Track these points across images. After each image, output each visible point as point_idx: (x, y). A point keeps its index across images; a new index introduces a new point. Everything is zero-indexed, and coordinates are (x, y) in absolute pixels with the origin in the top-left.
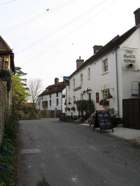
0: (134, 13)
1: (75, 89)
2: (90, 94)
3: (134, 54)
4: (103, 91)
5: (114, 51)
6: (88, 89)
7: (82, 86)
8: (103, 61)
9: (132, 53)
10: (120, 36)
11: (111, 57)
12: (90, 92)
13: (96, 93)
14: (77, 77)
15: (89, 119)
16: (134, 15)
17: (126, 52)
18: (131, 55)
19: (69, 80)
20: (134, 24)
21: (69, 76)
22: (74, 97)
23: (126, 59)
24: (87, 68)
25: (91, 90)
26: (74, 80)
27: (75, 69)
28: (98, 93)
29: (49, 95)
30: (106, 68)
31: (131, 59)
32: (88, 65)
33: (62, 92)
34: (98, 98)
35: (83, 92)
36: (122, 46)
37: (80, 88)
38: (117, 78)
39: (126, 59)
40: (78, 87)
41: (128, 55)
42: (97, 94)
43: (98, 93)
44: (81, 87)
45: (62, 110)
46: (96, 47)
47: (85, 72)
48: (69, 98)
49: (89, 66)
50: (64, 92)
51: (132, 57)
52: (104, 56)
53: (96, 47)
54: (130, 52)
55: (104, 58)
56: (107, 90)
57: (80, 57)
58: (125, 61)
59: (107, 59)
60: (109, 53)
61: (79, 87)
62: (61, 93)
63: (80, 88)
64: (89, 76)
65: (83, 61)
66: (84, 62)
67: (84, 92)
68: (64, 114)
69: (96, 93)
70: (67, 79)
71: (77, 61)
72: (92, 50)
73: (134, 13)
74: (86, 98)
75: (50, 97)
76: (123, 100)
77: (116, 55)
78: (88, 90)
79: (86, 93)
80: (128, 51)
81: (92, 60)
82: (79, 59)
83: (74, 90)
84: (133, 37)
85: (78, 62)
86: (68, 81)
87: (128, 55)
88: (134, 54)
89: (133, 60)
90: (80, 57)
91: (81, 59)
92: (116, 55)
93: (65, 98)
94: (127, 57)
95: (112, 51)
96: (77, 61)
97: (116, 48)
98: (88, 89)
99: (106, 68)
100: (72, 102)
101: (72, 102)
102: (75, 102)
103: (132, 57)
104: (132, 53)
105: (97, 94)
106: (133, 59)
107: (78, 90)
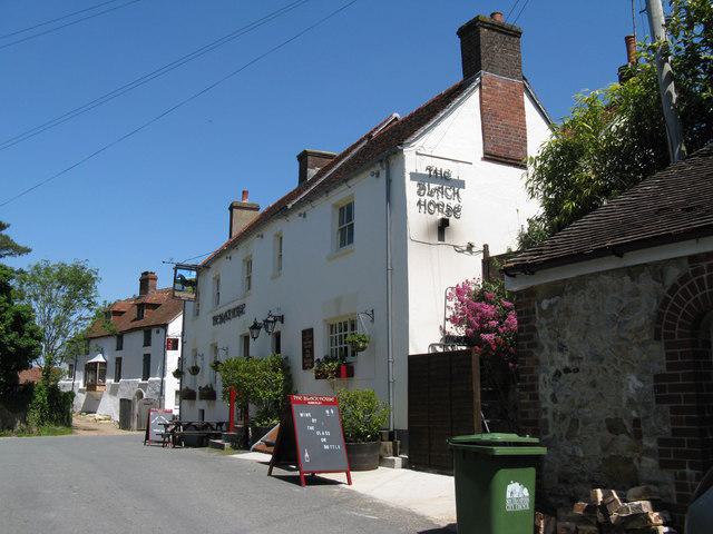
12: (278, 326)
13: (304, 332)
14: (231, 271)
21: (200, 262)
25: (282, 319)
30: (346, 235)
31: (446, 201)
37: (239, 311)
40: (231, 306)
42: (308, 335)
58: (423, 208)
63: (239, 311)
67: (256, 327)
69: (304, 332)
70: (191, 276)
81: (280, 210)
83: (215, 319)
105: (308, 335)
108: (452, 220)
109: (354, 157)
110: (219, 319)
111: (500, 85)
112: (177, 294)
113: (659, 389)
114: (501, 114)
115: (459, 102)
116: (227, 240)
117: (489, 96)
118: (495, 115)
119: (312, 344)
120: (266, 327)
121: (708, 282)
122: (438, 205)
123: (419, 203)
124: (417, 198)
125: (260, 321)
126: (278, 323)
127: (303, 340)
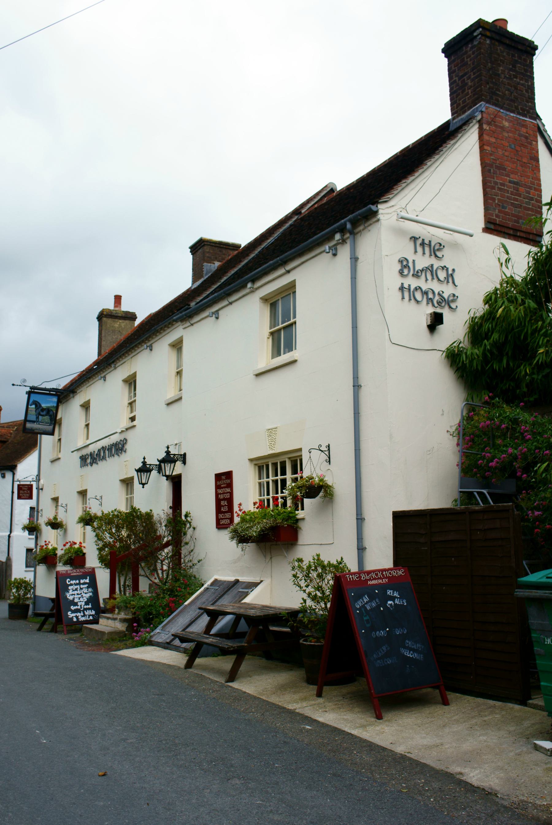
0: (444, 51)
1: (85, 452)
2: (176, 482)
3: (449, 259)
4: (262, 465)
5: (338, 236)
6: (168, 453)
7: (130, 436)
8: (265, 300)
9: (439, 254)
10: (339, 188)
11: (318, 281)
12: (178, 468)
13: (218, 477)
14: (107, 394)
15: (177, 624)
16: (442, 63)
17: (412, 244)
18: (437, 264)
19: (57, 408)
20: (441, 113)
21: (61, 384)
22: (83, 494)
23: (413, 283)
24: (162, 347)
25: (183, 458)
26: (86, 406)
27: (88, 353)
28: (229, 475)
29: (53, 596)
30: (283, 337)
31: (436, 287)
32: (176, 321)
33: (12, 468)
34: (230, 501)
35: (139, 471)
36: (389, 211)
37: (118, 448)
38: (357, 387)
39: (413, 283)
40: (106, 443)
41: (423, 261)
42: (224, 481)
43: (229, 475)
44: (124, 442)
45: (9, 559)
46: (201, 248)
47: (152, 364)
48: (56, 500)
49: (178, 332)
50: (26, 469)
51: (442, 275)
52: (274, 268)
53: (201, 248)
54: (434, 249)
55: (273, 284)
56: (282, 458)
57: (118, 299)
58: (406, 295)
59: (291, 288)
60: (309, 249)
61: (113, 445)
62: (9, 475)
63: (118, 448)
64: (492, 221)
65: (132, 317)
66: (137, 322)
67: (145, 469)
68: (22, 584)
69: (218, 477)
70: (49, 402)
71: (103, 317)
72: (187, 261)
73: (444, 51)
74: (153, 499)
75: (84, 530)
76: (400, 519)
77: (354, 259)
78: (169, 459)
79: (154, 473)
80: (423, 244)
81: (181, 310)
82: (110, 305)
83: (83, 459)
84: (413, 192)
85: (108, 321)
86: (48, 410)
87: (423, 261)
88: (449, 259)
89: (446, 296)
90: (118, 299)
91: (125, 307)
92: (354, 259)
93: (32, 503)
94: (416, 275)
95: (330, 237)
96: (103, 317)
97: (355, 223)
98: (168, 453)
99: (283, 337)
100: (71, 516)
101: (71, 516)
102: (87, 520)
103: (442, 275)
104: (439, 254)
105: (224, 481)
106: (447, 290)
107: (104, 458)
108: (446, 312)
109: (284, 234)
110: (89, 459)
111: (507, 124)
112: (28, 425)
113: (78, 551)
114: (509, 166)
115: (413, 180)
116: (94, 357)
117: (493, 140)
118: (501, 168)
119: (231, 493)
120: (160, 470)
121: (298, 506)
122: (426, 293)
123: (402, 288)
124: (398, 281)
125: (152, 460)
126: (179, 464)
127: (217, 487)
